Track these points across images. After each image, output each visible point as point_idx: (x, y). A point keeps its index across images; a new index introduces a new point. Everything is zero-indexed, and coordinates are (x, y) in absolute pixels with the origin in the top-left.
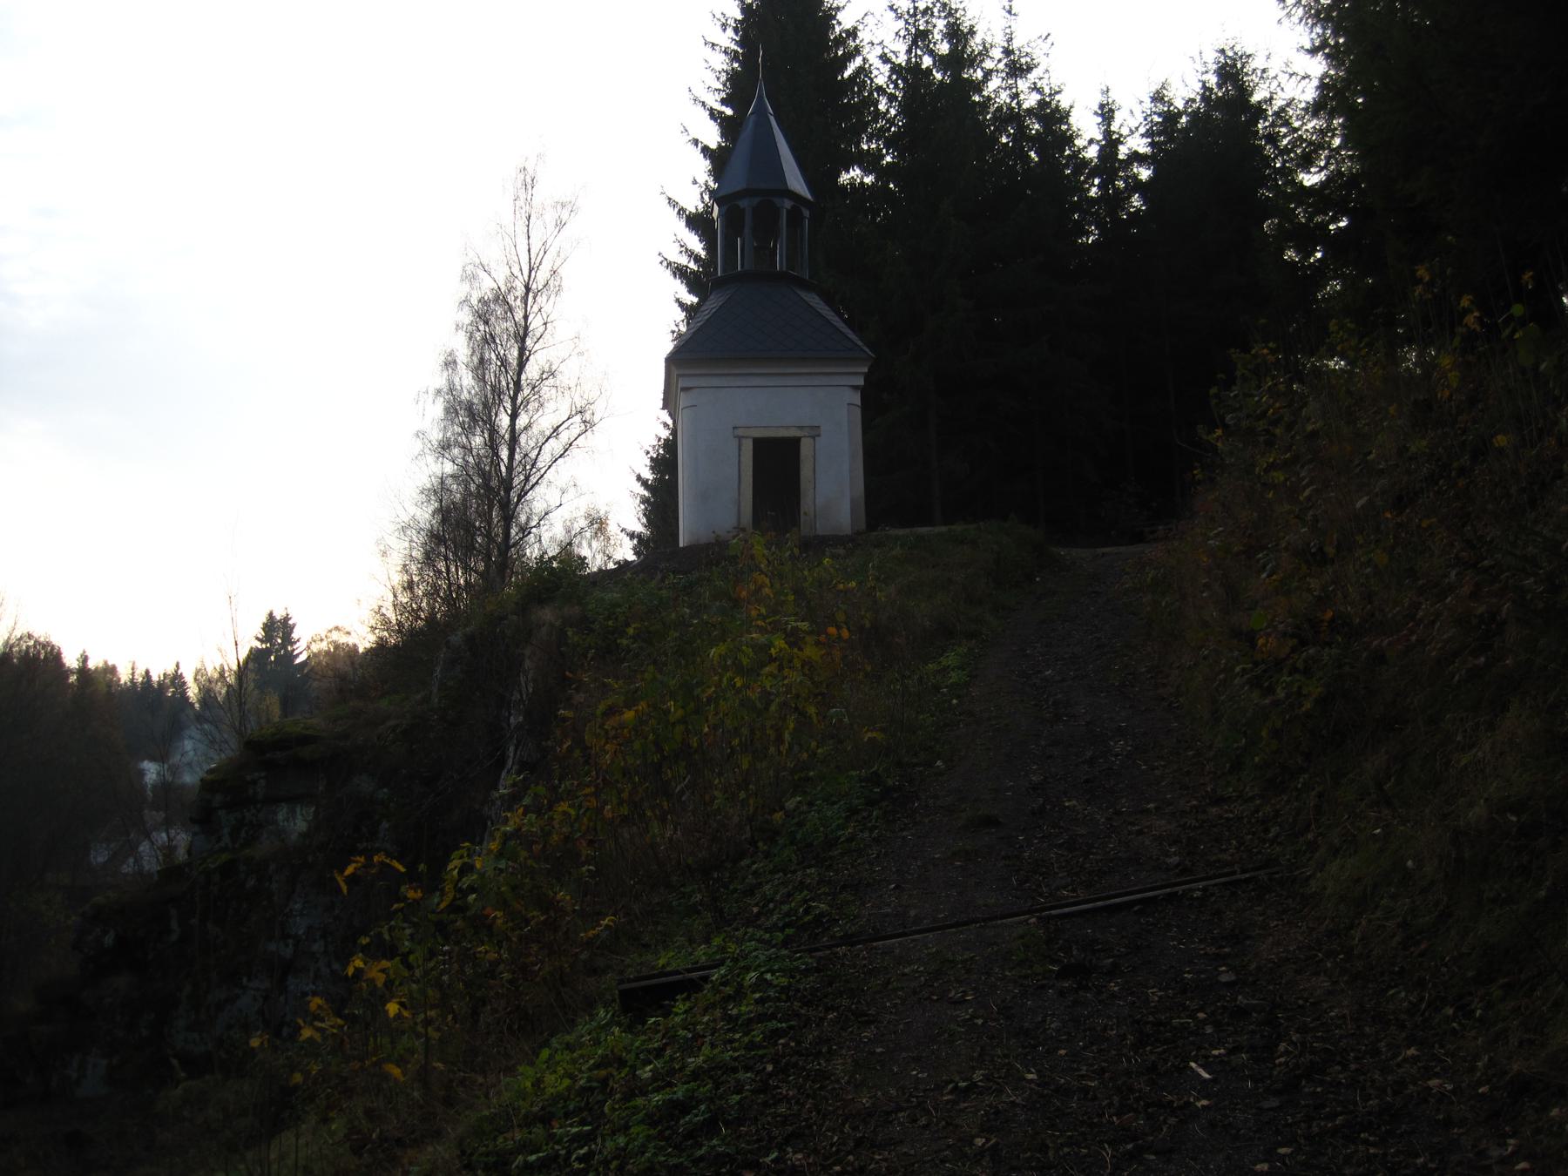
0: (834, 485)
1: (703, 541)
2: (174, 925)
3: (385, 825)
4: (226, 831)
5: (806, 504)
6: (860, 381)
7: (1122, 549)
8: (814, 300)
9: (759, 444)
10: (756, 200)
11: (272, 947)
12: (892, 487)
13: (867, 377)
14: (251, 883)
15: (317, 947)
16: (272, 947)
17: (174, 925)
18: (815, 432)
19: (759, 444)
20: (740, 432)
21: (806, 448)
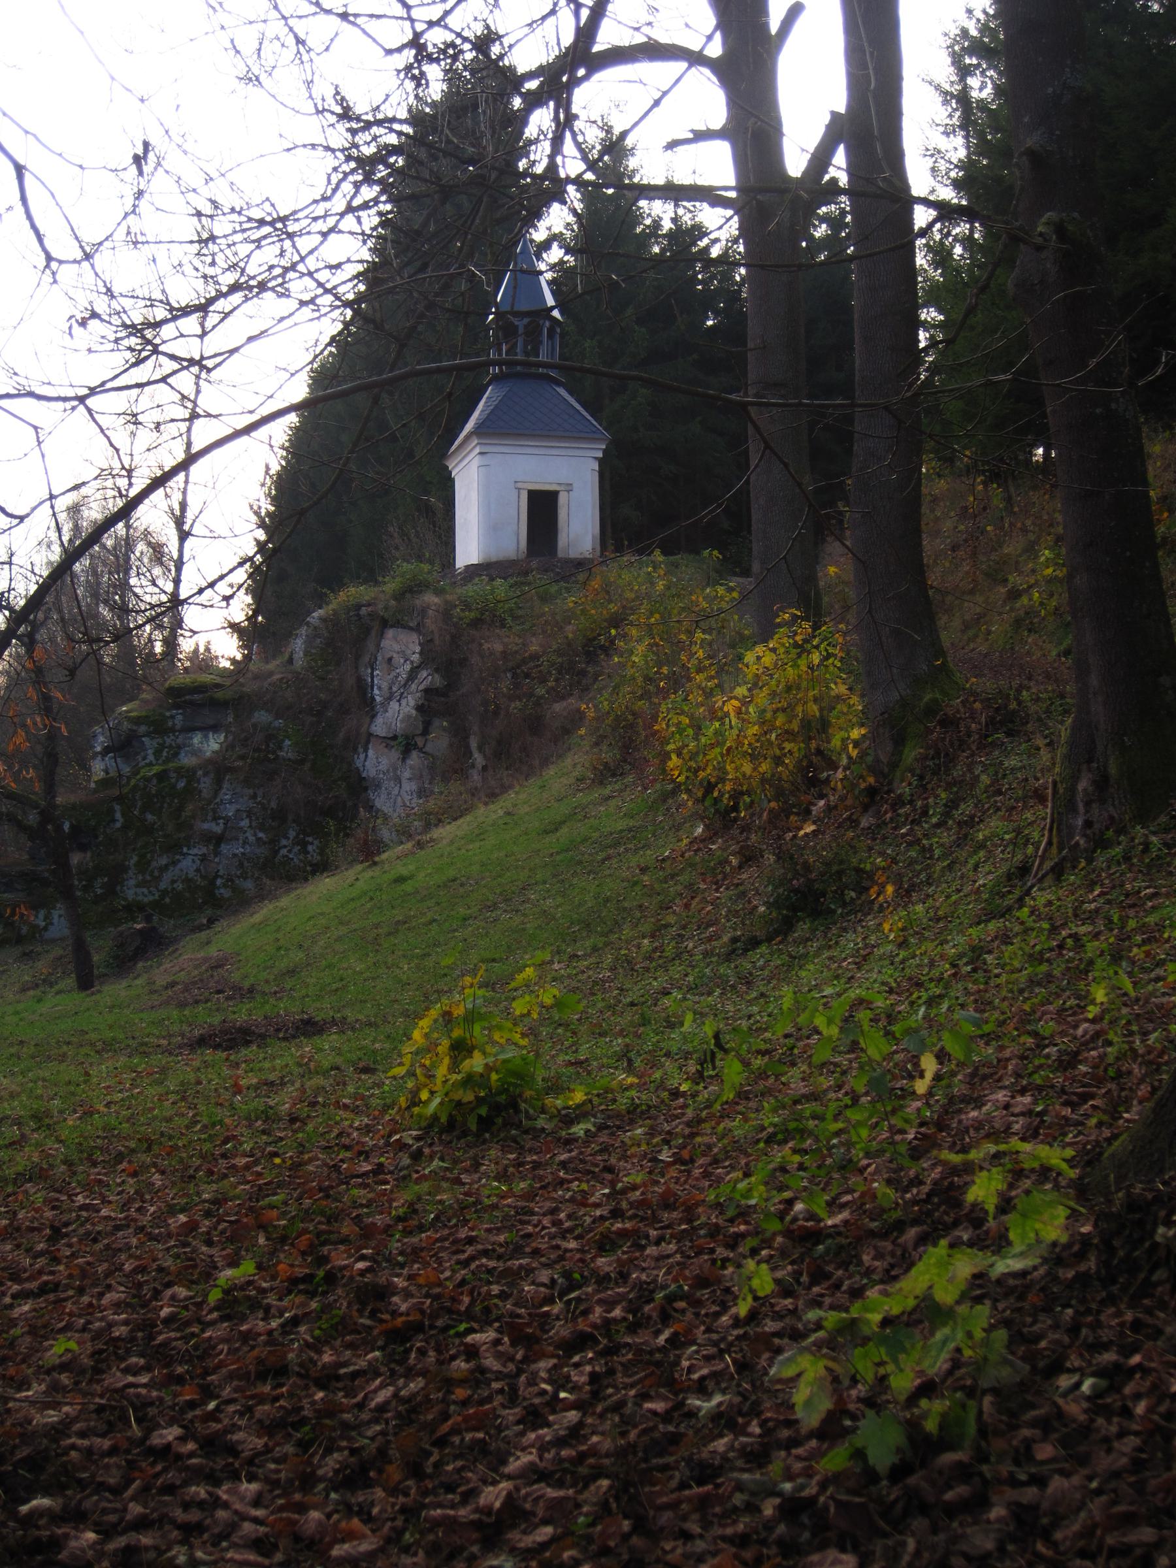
0: (580, 527)
1: (494, 559)
2: (118, 815)
3: (287, 742)
4: (150, 752)
5: (562, 541)
6: (600, 455)
7: (756, 547)
8: (562, 391)
9: (531, 494)
10: (526, 321)
11: (206, 826)
12: (621, 529)
13: (605, 451)
14: (181, 784)
15: (245, 823)
16: (206, 826)
17: (118, 815)
18: (569, 488)
19: (531, 494)
20: (519, 485)
21: (562, 499)
